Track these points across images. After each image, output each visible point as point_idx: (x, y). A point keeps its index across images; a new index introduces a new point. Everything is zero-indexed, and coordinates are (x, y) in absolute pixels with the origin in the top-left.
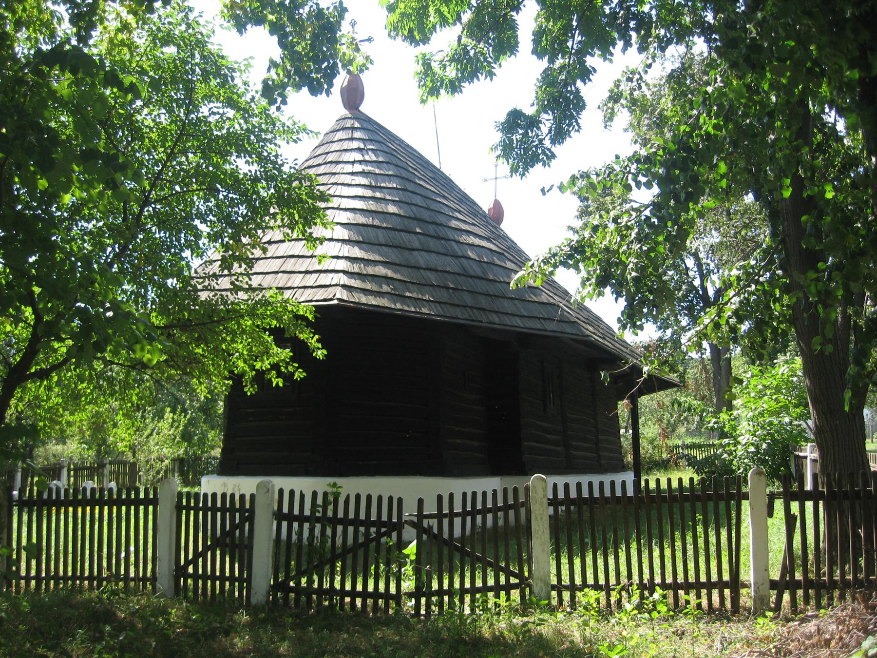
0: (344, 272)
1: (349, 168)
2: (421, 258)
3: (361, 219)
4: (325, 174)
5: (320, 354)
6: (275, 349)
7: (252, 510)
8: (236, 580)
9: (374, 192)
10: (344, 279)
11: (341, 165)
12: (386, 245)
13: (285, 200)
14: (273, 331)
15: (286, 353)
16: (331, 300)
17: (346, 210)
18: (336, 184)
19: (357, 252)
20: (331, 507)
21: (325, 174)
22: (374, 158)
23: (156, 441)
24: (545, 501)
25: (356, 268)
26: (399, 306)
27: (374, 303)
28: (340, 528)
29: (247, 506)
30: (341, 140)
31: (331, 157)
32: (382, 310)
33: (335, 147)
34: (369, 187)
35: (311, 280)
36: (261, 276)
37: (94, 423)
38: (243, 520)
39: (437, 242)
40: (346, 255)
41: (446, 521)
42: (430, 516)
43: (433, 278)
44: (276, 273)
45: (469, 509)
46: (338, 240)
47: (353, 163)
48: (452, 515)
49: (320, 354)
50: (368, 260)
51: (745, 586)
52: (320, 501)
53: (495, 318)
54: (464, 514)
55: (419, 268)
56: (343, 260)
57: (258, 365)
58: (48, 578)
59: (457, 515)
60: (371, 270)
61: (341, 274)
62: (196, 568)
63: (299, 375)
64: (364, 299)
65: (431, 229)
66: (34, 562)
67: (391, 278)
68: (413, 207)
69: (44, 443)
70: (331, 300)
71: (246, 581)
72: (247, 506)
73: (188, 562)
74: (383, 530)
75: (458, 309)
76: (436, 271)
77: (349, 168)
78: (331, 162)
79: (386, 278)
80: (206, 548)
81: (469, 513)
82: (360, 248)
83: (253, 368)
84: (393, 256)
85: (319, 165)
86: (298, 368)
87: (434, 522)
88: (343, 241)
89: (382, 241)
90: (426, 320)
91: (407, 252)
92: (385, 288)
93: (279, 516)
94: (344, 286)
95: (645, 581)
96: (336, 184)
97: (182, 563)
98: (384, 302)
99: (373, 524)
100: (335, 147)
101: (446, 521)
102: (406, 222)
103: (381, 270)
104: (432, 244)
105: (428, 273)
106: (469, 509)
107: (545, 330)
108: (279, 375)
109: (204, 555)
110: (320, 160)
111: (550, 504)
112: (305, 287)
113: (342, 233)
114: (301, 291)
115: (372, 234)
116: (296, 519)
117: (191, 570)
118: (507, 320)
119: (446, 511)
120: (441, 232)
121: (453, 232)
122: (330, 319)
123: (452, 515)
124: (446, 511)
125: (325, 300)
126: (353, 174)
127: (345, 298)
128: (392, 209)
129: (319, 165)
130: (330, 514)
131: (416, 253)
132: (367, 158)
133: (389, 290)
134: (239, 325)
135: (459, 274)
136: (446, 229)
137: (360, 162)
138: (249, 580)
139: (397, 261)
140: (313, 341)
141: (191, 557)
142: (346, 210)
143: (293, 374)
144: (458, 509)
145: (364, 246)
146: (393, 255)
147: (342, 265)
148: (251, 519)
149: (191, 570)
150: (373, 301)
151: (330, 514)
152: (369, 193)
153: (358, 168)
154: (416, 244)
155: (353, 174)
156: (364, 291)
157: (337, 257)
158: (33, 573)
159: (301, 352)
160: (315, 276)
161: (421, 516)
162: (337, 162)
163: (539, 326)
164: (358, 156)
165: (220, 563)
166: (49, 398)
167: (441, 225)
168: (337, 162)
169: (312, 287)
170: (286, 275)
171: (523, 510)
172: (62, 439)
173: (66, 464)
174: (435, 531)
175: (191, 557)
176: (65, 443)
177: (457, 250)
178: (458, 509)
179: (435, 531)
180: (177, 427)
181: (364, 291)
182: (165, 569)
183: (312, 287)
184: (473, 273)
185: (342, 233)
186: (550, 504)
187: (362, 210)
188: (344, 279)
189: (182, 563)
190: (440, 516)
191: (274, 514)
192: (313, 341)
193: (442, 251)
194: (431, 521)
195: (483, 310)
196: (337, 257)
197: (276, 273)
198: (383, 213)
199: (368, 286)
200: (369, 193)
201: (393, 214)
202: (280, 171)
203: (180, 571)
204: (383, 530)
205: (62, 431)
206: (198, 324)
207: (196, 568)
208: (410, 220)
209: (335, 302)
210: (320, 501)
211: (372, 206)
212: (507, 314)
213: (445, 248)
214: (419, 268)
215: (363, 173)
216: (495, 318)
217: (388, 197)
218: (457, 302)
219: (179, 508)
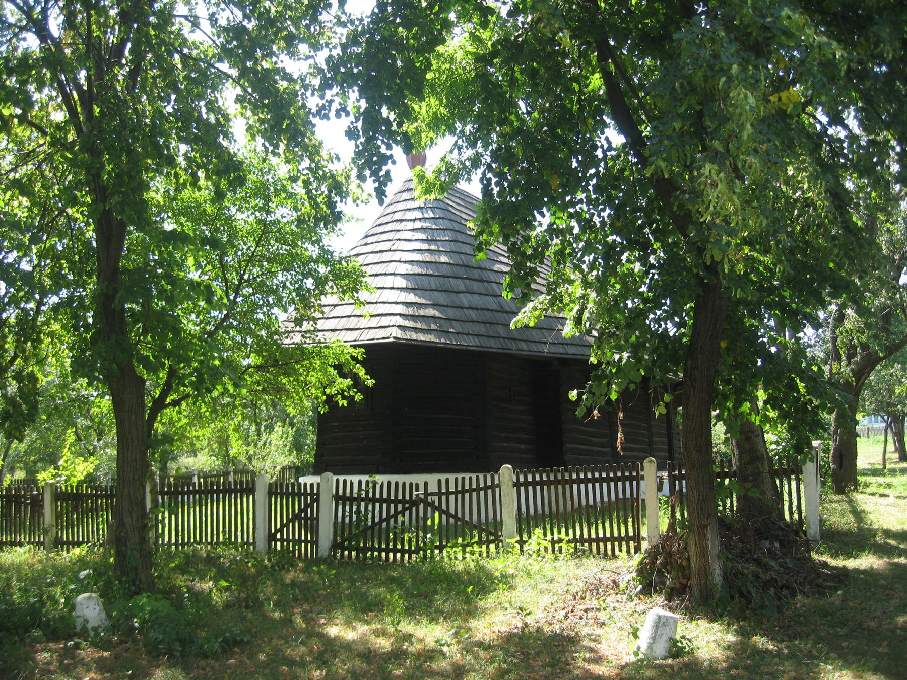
0: (400, 315)
1: (410, 225)
2: (465, 299)
3: (417, 270)
4: (391, 231)
5: (370, 383)
6: (339, 380)
7: (318, 494)
8: (309, 542)
9: (430, 245)
10: (399, 321)
11: (404, 223)
12: (436, 290)
13: (337, 275)
14: (335, 367)
15: (349, 382)
16: (388, 338)
17: (405, 262)
18: (399, 240)
19: (412, 298)
20: (371, 490)
21: (391, 231)
22: (432, 215)
23: (274, 453)
24: (511, 483)
25: (410, 311)
26: (443, 341)
27: (423, 339)
28: (377, 505)
29: (315, 491)
30: (406, 200)
31: (397, 216)
32: (428, 344)
33: (401, 206)
34: (427, 241)
35: (375, 322)
36: (337, 320)
37: (219, 437)
38: (313, 501)
39: (480, 284)
40: (403, 300)
41: (444, 498)
42: (432, 494)
43: (473, 315)
44: (349, 316)
45: (460, 489)
46: (398, 288)
47: (414, 220)
48: (448, 493)
49: (370, 383)
50: (420, 304)
51: (644, 539)
52: (364, 487)
53: (524, 346)
54: (456, 493)
55: (462, 308)
56: (400, 305)
57: (328, 391)
58: (183, 544)
59: (452, 493)
60: (422, 312)
61: (398, 317)
62: (282, 535)
63: (358, 397)
64: (414, 336)
65: (476, 274)
66: (173, 517)
67: (439, 318)
68: (462, 256)
69: (175, 459)
70: (388, 338)
71: (315, 542)
72: (315, 491)
73: (277, 531)
74: (407, 505)
75: (492, 340)
76: (477, 309)
77: (410, 225)
78: (397, 221)
79: (434, 317)
80: (289, 521)
81: (459, 492)
82: (415, 295)
83: (324, 393)
84: (442, 299)
85: (387, 223)
86: (356, 393)
87: (436, 498)
88: (401, 289)
89: (434, 287)
90: (465, 350)
91: (454, 295)
92: (433, 327)
93: (337, 498)
94: (399, 327)
95: (578, 537)
96: (399, 240)
97: (273, 531)
98: (431, 338)
99: (400, 502)
100: (401, 206)
101: (444, 498)
102: (455, 269)
103: (431, 312)
104: (476, 286)
105: (470, 311)
106: (460, 489)
107: (567, 354)
108: (344, 398)
109: (287, 525)
110: (388, 219)
111: (514, 486)
112: (370, 328)
113: (401, 282)
114: (367, 331)
115: (425, 282)
116: (385, 501)
117: (278, 536)
118: (534, 347)
119: (444, 490)
120: (485, 275)
121: (495, 275)
122: (377, 355)
123: (448, 493)
124: (444, 490)
125: (384, 338)
126: (413, 230)
127: (399, 336)
128: (444, 259)
129: (387, 223)
130: (371, 495)
131: (461, 295)
132: (426, 216)
133: (436, 328)
134: (311, 363)
135: (496, 311)
136: (489, 272)
137: (420, 219)
138: (317, 543)
139: (445, 303)
140: (362, 372)
141: (278, 527)
142: (405, 262)
143: (354, 397)
144: (452, 489)
145: (418, 292)
146: (441, 298)
147: (400, 309)
148: (318, 500)
149: (278, 536)
150: (421, 337)
151: (371, 495)
152: (425, 246)
153: (418, 225)
154: (462, 288)
155: (413, 230)
156: (415, 330)
157: (396, 303)
158: (173, 541)
159: (357, 383)
160: (378, 318)
161: (426, 494)
162: (402, 221)
163: (561, 350)
164: (418, 214)
165: (295, 531)
166: (180, 420)
167: (485, 269)
168: (402, 221)
169: (375, 328)
170: (356, 319)
171: (497, 490)
172: (194, 452)
173: (196, 473)
174: (437, 504)
175: (278, 527)
176: (196, 456)
177: (497, 290)
178: (452, 489)
179: (437, 504)
180: (286, 438)
181: (415, 330)
182: (262, 535)
183: (375, 328)
184: (508, 309)
185: (401, 282)
186: (514, 486)
187: (419, 262)
188: (399, 321)
189: (273, 531)
190: (439, 494)
191: (333, 496)
192: (362, 372)
193: (483, 292)
194: (434, 498)
195: (514, 339)
196: (396, 303)
197: (349, 316)
198: (436, 263)
199: (419, 326)
200: (425, 246)
201: (447, 264)
202: (332, 257)
203: (271, 537)
204: (407, 505)
205: (193, 445)
206: (282, 361)
207: (282, 535)
208: (458, 268)
209: (391, 340)
210: (364, 487)
211: (427, 257)
212: (535, 342)
213: (487, 289)
214: (462, 308)
215: (422, 229)
216: (524, 346)
217: (441, 249)
218: (492, 334)
219: (270, 494)
